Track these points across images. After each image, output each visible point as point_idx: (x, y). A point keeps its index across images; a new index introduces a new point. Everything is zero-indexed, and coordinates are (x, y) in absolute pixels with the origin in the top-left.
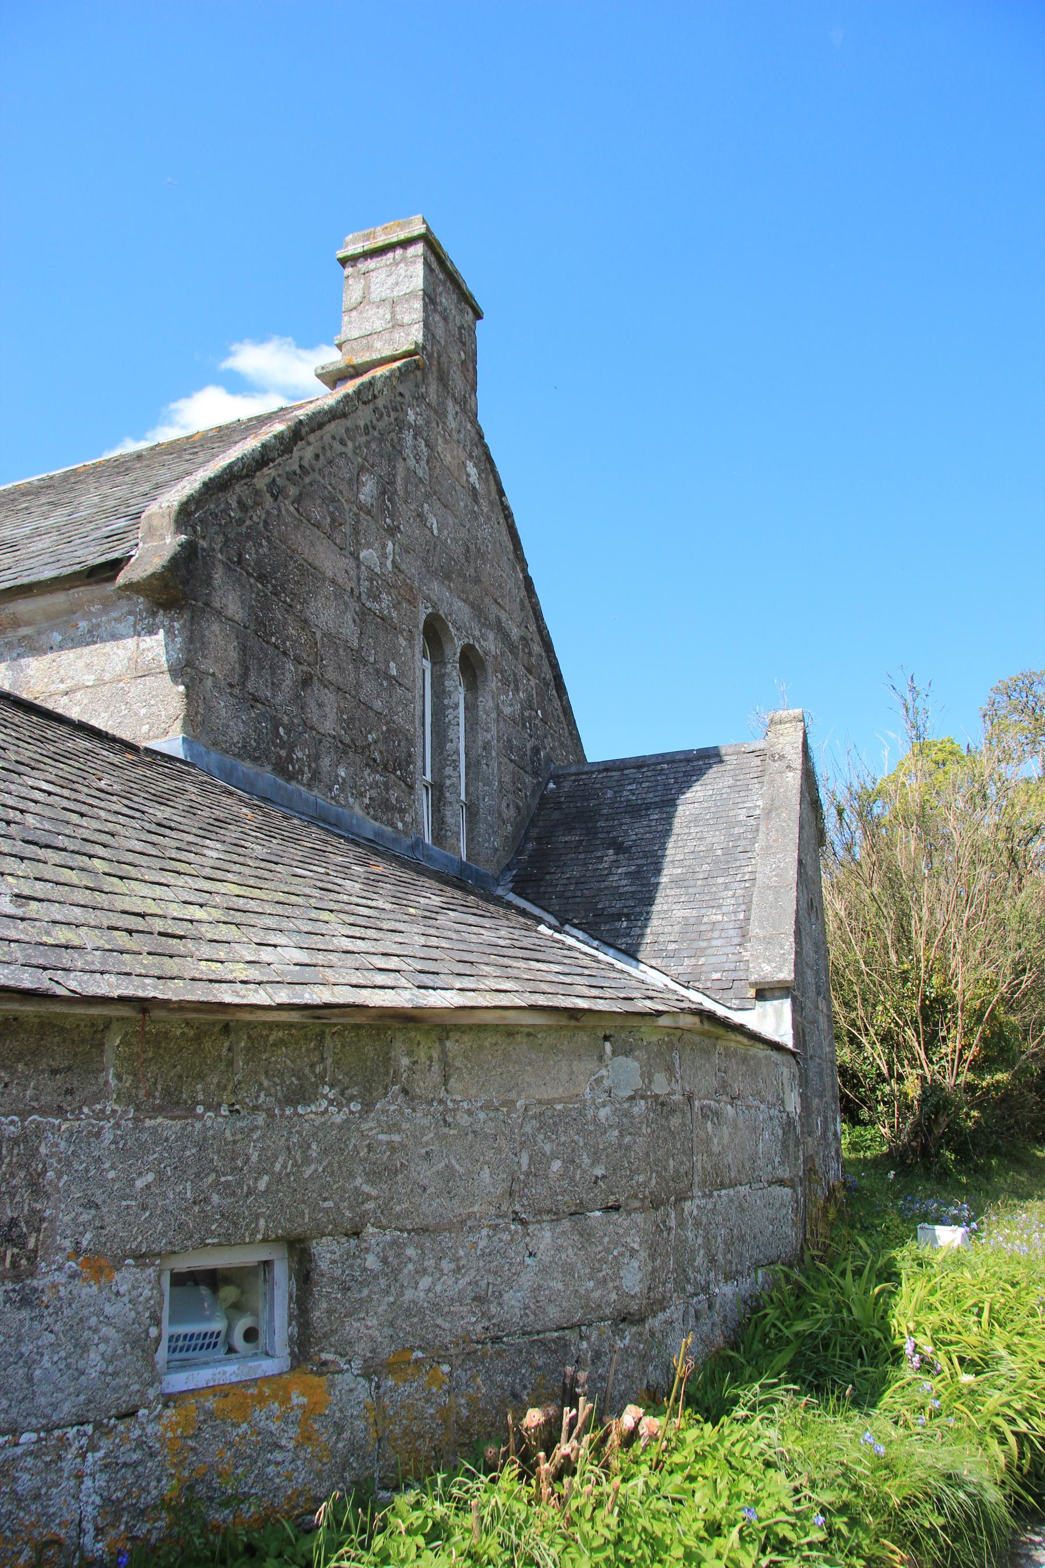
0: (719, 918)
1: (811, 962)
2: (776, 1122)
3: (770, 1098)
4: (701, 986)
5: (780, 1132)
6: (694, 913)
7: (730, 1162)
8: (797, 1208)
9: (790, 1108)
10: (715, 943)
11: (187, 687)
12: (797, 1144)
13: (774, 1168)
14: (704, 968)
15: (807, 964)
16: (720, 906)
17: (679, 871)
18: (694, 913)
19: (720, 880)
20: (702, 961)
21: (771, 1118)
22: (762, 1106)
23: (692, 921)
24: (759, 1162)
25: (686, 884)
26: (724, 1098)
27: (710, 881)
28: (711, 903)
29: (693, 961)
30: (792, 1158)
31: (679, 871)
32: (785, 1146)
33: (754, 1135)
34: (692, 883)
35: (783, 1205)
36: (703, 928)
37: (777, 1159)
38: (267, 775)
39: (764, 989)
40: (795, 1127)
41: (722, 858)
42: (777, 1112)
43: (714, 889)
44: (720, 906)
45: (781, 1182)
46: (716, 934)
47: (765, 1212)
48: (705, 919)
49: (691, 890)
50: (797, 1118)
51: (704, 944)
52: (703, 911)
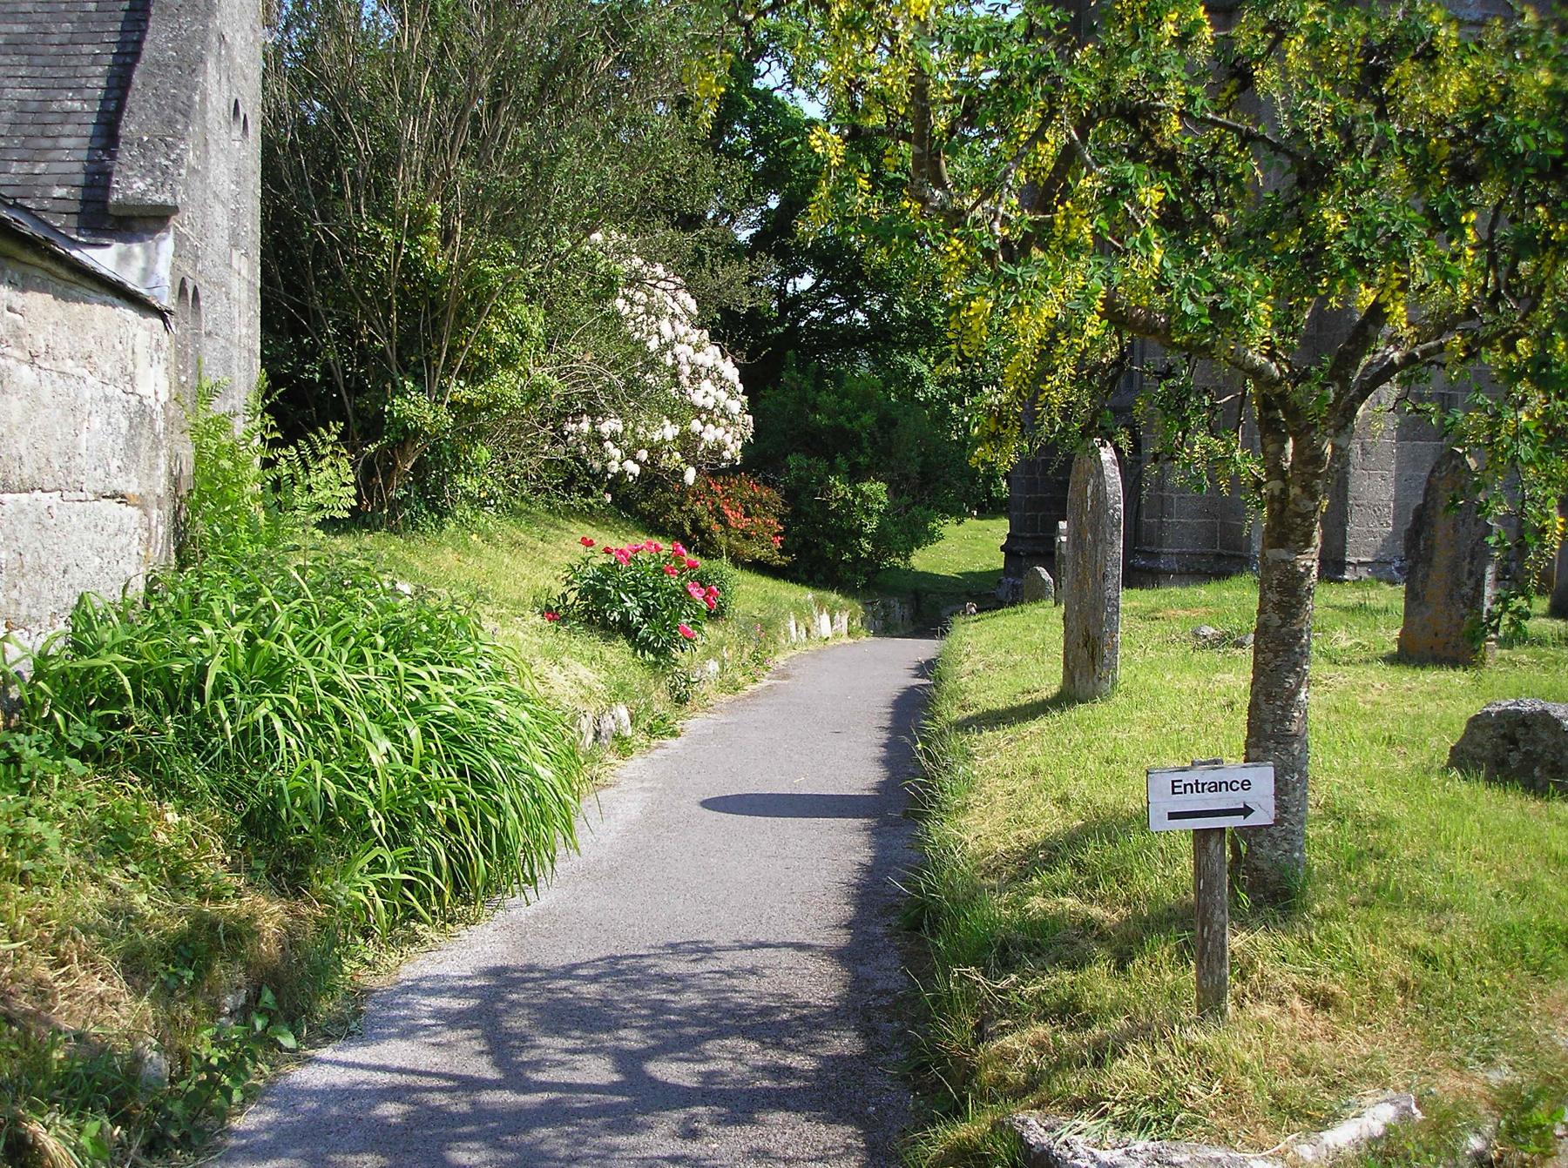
0: (77, 105)
1: (225, 195)
2: (116, 406)
3: (107, 368)
4: (33, 206)
5: (125, 424)
6: (38, 95)
7: (23, 453)
8: (149, 540)
9: (144, 389)
10: (64, 142)
11: (786, 456)
12: (156, 445)
13: (108, 475)
14: (42, 180)
15: (216, 196)
16: (80, 89)
17: (23, 28)
18: (38, 95)
19: (86, 49)
20: (40, 168)
21: (107, 399)
22: (90, 380)
23: (33, 106)
24: (78, 459)
25: (30, 49)
26: (17, 353)
27: (71, 49)
28: (67, 83)
29: (26, 167)
30: (144, 464)
31: (23, 28)
32: (131, 447)
33: (71, 419)
34: (40, 49)
35: (120, 531)
36: (50, 119)
37: (115, 463)
38: (576, 499)
39: (132, 218)
40: (152, 420)
41: (95, 16)
42: (118, 391)
43: (75, 62)
44: (80, 89)
45: (120, 497)
46: (68, 129)
47: (89, 536)
48: (55, 106)
49: (37, 60)
50: (158, 408)
51: (47, 143)
52: (53, 93)
